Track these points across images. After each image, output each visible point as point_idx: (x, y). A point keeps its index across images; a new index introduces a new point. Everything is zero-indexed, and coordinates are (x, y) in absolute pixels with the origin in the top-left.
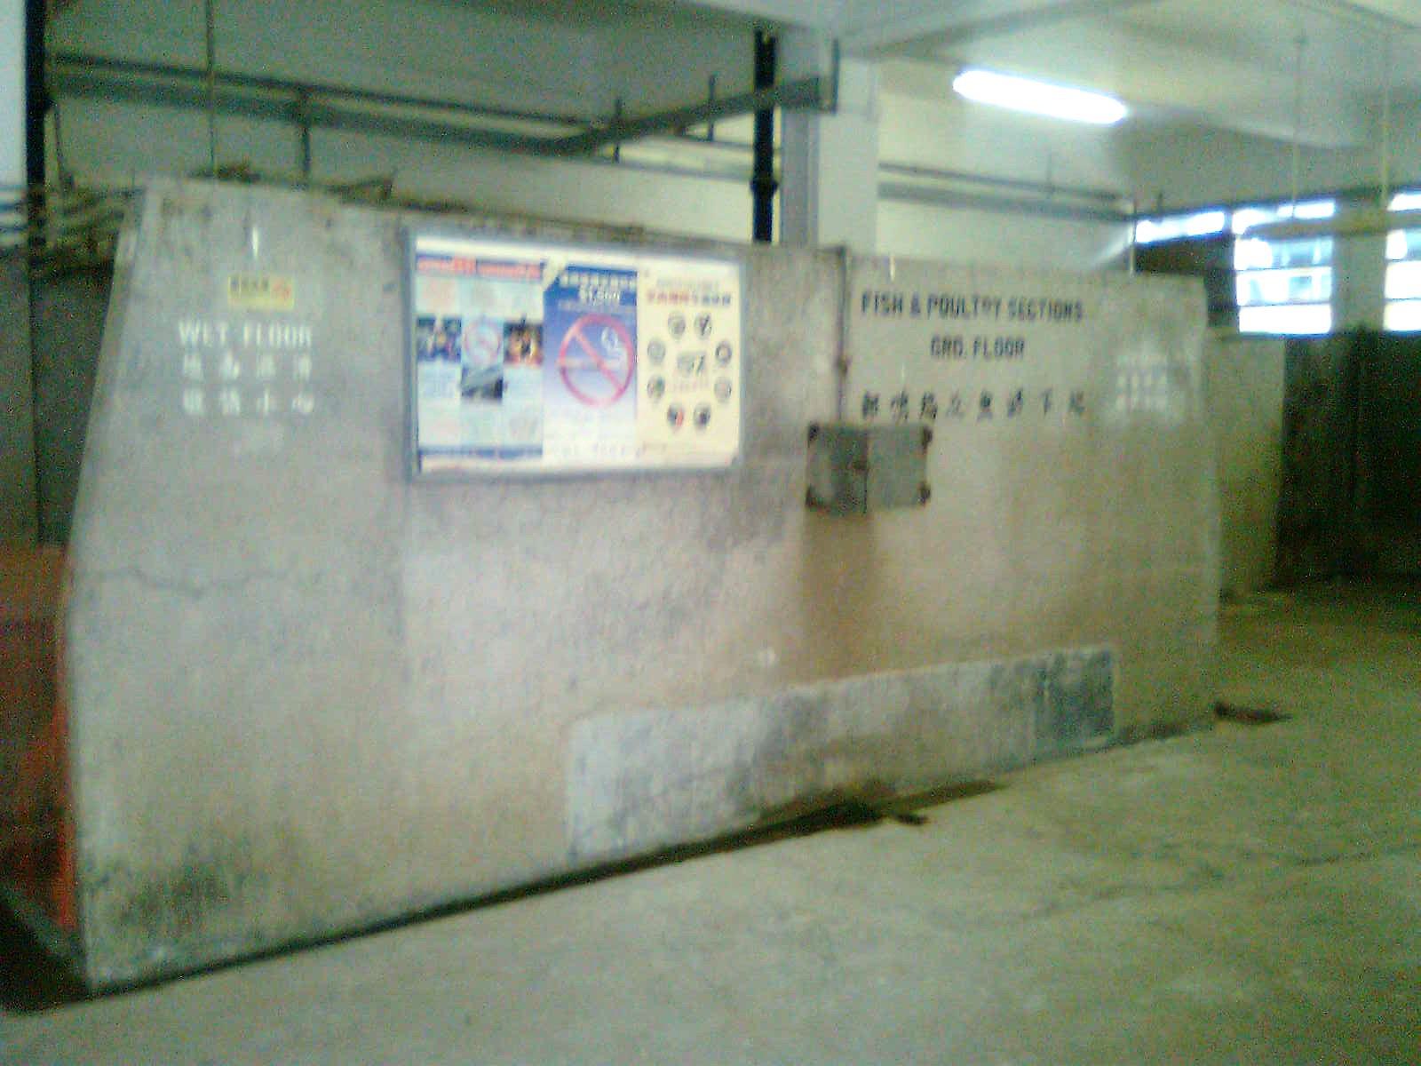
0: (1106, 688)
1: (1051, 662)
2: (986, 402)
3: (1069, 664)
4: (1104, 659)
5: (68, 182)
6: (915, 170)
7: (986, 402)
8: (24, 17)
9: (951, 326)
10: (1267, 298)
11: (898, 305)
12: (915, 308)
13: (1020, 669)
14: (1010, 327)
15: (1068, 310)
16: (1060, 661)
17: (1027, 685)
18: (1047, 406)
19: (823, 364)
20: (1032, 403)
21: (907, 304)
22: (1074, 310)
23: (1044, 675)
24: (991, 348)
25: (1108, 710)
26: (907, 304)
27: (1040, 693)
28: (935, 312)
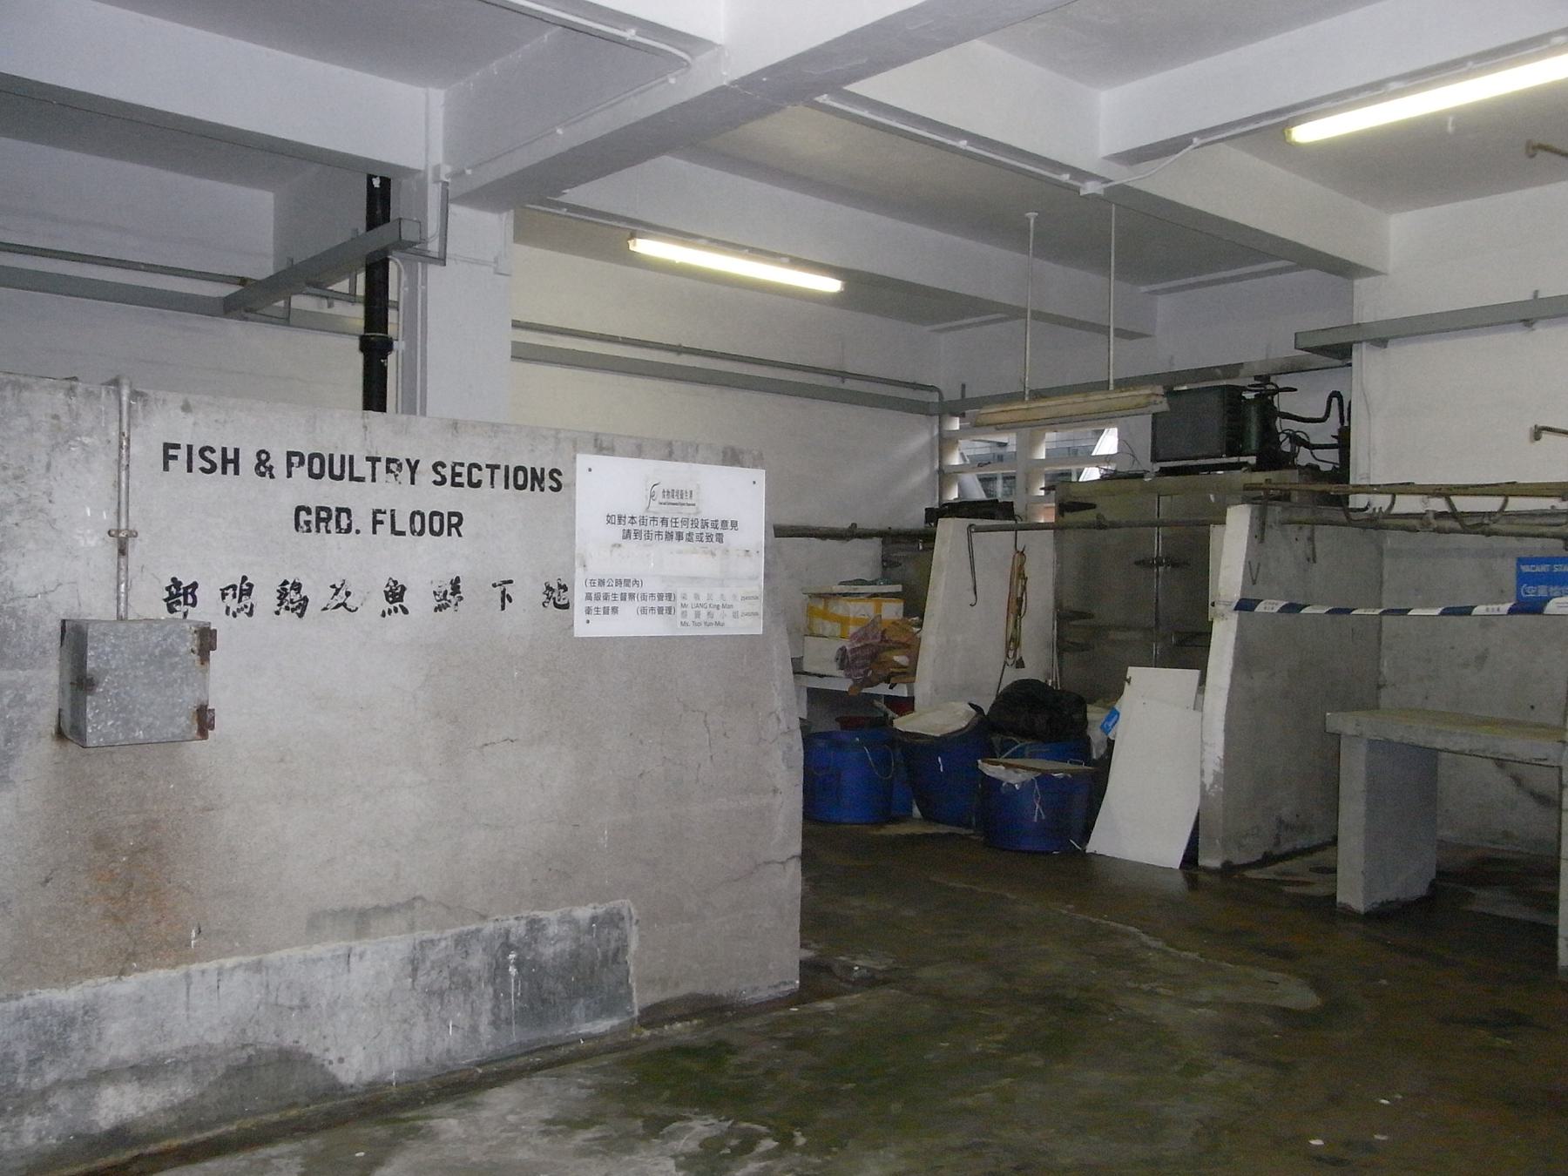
0: (616, 956)
1: (519, 929)
2: (395, 594)
3: (552, 930)
4: (613, 920)
5: (1484, 751)
6: (679, 350)
7: (395, 594)
8: (736, 275)
9: (329, 493)
10: (1109, 517)
11: (231, 461)
12: (263, 465)
13: (462, 941)
14: (446, 499)
15: (537, 479)
16: (535, 926)
17: (477, 961)
18: (505, 598)
19: (93, 542)
20: (477, 594)
21: (248, 461)
22: (548, 482)
23: (507, 947)
24: (403, 524)
25: (624, 982)
26: (248, 461)
27: (499, 969)
28: (301, 473)
